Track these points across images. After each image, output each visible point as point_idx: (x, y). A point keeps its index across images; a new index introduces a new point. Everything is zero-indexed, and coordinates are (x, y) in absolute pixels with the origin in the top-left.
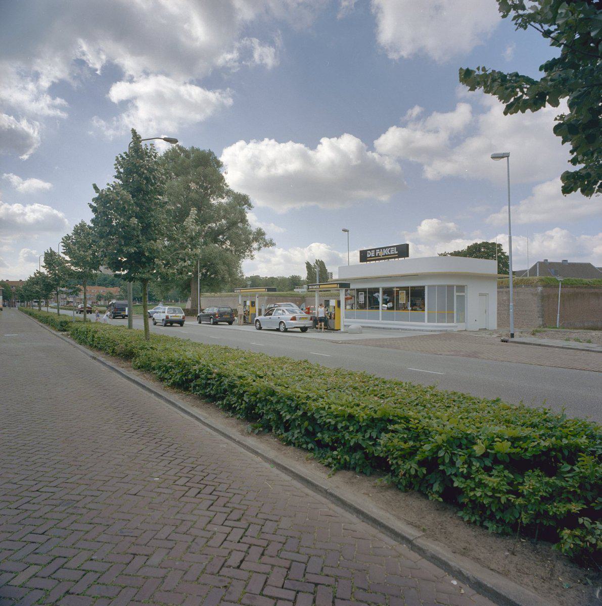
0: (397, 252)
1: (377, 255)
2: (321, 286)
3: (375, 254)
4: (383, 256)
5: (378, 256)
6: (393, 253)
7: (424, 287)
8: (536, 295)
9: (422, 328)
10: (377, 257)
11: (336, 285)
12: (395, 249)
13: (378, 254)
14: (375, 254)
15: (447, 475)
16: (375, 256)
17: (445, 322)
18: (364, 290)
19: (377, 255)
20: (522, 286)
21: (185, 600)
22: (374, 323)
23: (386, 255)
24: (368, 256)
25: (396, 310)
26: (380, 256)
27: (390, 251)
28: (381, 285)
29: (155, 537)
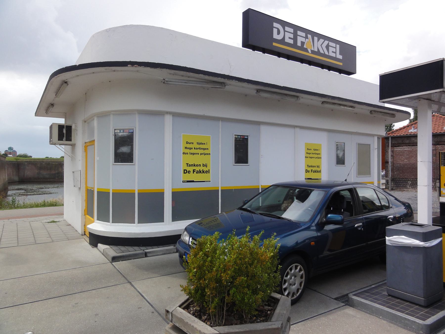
0: (340, 57)
4: (313, 52)
5: (302, 48)
6: (334, 55)
13: (303, 43)
19: (299, 44)
23: (318, 53)
24: (275, 36)
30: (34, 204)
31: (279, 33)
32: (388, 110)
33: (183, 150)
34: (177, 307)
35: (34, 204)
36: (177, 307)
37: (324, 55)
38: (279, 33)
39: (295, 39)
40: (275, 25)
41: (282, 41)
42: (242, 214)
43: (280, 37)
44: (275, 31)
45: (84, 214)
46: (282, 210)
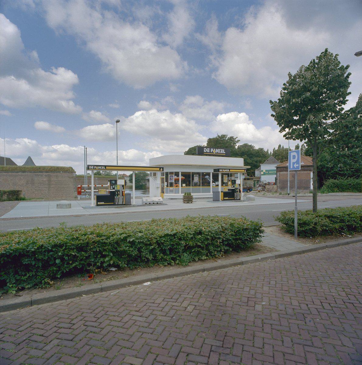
0: (225, 153)
1: (211, 152)
2: (231, 170)
3: (210, 151)
4: (215, 153)
5: (212, 153)
6: (222, 153)
7: (210, 173)
8: (72, 177)
9: (204, 197)
10: (211, 153)
11: (243, 171)
12: (224, 151)
13: (212, 151)
14: (210, 151)
15: (33, 265)
16: (210, 152)
17: (200, 193)
18: (198, 174)
19: (211, 152)
20: (61, 172)
21: (271, 344)
22: (206, 195)
23: (217, 153)
24: (205, 151)
25: (202, 186)
26: (214, 153)
27: (220, 151)
28: (180, 171)
29: (117, 344)
30: (173, 220)
31: (205, 150)
32: (93, 290)
33: (291, 73)
34: (134, 206)
35: (173, 220)
36: (134, 206)
37: (219, 153)
38: (205, 150)
39: (210, 150)
40: (204, 149)
41: (207, 152)
42: (116, 119)
43: (206, 151)
44: (204, 150)
45: (156, 218)
46: (47, 252)
